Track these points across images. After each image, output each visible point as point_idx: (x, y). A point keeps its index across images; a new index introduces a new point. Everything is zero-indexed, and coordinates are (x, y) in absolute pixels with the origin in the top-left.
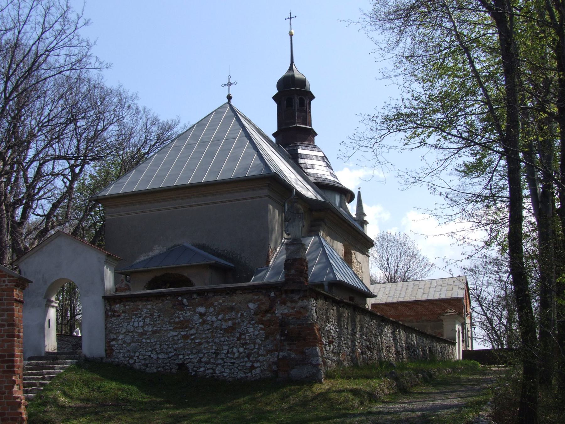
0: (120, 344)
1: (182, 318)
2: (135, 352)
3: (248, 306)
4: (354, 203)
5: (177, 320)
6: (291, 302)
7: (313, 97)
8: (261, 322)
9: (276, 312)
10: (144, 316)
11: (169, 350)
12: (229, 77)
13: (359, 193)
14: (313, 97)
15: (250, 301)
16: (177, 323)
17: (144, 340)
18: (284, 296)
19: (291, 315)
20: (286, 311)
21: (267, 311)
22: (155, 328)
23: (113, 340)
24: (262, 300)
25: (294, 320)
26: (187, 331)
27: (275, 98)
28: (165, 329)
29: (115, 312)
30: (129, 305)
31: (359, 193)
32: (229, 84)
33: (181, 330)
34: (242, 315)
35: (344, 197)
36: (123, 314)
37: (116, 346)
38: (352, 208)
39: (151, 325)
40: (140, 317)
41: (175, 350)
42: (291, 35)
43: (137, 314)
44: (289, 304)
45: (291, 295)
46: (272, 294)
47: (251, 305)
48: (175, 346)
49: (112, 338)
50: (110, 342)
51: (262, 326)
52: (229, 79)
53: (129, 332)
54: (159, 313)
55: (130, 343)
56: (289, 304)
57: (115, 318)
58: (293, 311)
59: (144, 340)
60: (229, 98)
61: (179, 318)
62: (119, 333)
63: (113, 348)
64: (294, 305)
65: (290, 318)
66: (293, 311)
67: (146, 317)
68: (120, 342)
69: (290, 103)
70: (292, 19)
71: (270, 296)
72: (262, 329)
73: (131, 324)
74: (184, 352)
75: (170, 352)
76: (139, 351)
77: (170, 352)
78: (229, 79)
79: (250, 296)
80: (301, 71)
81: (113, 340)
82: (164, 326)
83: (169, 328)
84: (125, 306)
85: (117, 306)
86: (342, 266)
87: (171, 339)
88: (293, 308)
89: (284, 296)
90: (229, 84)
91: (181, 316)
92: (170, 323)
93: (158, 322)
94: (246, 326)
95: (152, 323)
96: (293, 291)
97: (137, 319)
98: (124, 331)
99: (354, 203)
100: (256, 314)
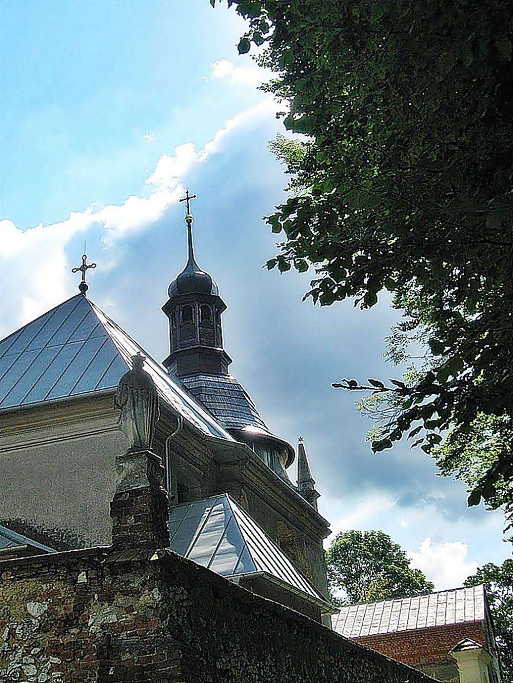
3: (26, 609)
4: (294, 466)
6: (125, 593)
7: (222, 306)
8: (54, 649)
9: (90, 622)
12: (84, 257)
13: (301, 447)
14: (222, 306)
15: (32, 597)
18: (108, 580)
19: (123, 628)
20: (113, 618)
21: (68, 622)
24: (57, 592)
25: (134, 639)
27: (167, 309)
31: (301, 447)
32: (84, 268)
34: (12, 633)
35: (277, 455)
38: (292, 474)
42: (189, 222)
44: (120, 600)
45: (126, 577)
46: (82, 578)
47: (34, 608)
51: (56, 660)
52: (84, 261)
56: (120, 600)
58: (130, 617)
60: (83, 287)
64: (131, 601)
65: (123, 635)
66: (130, 617)
69: (188, 315)
70: (186, 197)
71: (76, 581)
72: (56, 667)
78: (84, 261)
79: (31, 585)
80: (204, 267)
86: (303, 583)
88: (130, 610)
89: (108, 580)
90: (84, 268)
94: (20, 662)
96: (127, 567)
99: (294, 466)
100: (42, 629)
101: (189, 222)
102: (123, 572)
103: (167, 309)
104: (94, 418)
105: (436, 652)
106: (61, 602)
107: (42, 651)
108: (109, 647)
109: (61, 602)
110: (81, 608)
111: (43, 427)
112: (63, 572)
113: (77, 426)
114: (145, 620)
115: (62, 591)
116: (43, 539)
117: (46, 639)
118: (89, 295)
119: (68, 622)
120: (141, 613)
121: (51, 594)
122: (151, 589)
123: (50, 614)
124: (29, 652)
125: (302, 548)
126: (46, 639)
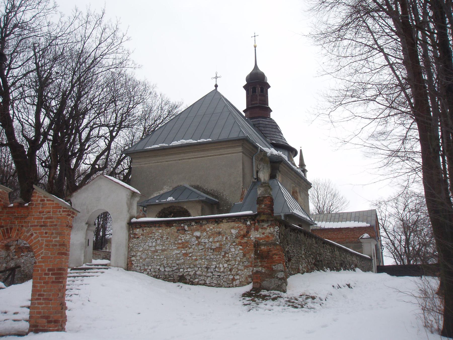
0: (138, 260)
1: (183, 241)
2: (148, 266)
3: (231, 231)
5: (180, 241)
6: (262, 229)
8: (240, 244)
9: (251, 236)
10: (156, 238)
11: (173, 265)
13: (301, 150)
15: (233, 228)
16: (180, 244)
17: (155, 257)
18: (257, 224)
19: (262, 239)
20: (258, 236)
21: (244, 236)
22: (163, 248)
23: (133, 256)
24: (241, 227)
26: (187, 250)
27: (245, 87)
28: (171, 248)
29: (135, 234)
30: (146, 230)
31: (301, 150)
32: (216, 77)
33: (182, 249)
36: (141, 237)
37: (135, 261)
39: (161, 245)
40: (154, 239)
41: (177, 265)
42: (255, 47)
43: (151, 237)
44: (260, 230)
47: (233, 231)
48: (178, 262)
49: (132, 254)
50: (131, 257)
51: (241, 247)
52: (216, 74)
53: (145, 250)
54: (167, 236)
55: (145, 259)
56: (260, 230)
57: (135, 240)
59: (155, 257)
60: (216, 86)
61: (182, 240)
62: (138, 251)
63: (133, 262)
64: (264, 231)
65: (261, 241)
67: (158, 239)
68: (138, 258)
69: (254, 91)
72: (241, 249)
73: (147, 244)
74: (184, 267)
75: (174, 267)
76: (152, 265)
77: (174, 267)
78: (216, 74)
79: (232, 224)
80: (262, 68)
81: (133, 256)
82: (170, 246)
83: (174, 248)
84: (143, 231)
85: (138, 230)
87: (175, 256)
88: (263, 234)
89: (257, 224)
90: (216, 77)
91: (183, 238)
92: (175, 244)
93: (166, 243)
94: (230, 247)
95: (162, 243)
97: (151, 240)
98: (141, 249)
100: (236, 237)
101: (255, 47)
102: (262, 222)
103: (245, 87)
104: (227, 148)
105: (353, 238)
106: (242, 230)
107: (236, 244)
108: (258, 244)
109: (242, 230)
110: (248, 232)
111: (208, 150)
112: (242, 221)
113: (221, 151)
114: (268, 237)
115: (242, 227)
116: (208, 193)
117: (238, 241)
118: (219, 89)
119: (244, 236)
120: (267, 235)
121: (238, 227)
122: (270, 228)
123: (238, 233)
124: (232, 244)
125: (300, 194)
126: (238, 241)
